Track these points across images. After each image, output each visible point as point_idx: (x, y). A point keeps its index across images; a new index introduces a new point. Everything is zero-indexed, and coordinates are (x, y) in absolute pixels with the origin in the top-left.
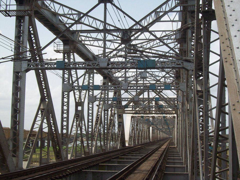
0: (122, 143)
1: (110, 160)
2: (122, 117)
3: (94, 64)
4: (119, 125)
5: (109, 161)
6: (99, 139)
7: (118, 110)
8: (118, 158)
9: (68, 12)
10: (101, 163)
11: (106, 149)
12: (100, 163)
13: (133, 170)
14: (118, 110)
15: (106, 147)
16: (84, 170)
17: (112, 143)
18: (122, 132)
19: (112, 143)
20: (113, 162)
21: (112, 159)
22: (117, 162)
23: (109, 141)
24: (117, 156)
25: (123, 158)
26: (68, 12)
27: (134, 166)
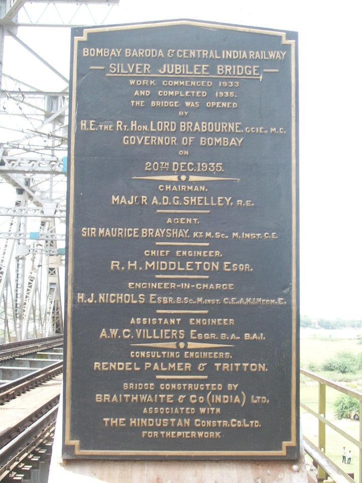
0: (55, 325)
1: (14, 358)
2: (56, 272)
3: (53, 163)
4: (51, 289)
5: (11, 361)
6: (32, 316)
7: (48, 259)
8: (34, 355)
9: (64, 78)
10: (40, 351)
11: (19, 337)
12: (17, 357)
13: (43, 379)
14: (48, 259)
15: (18, 334)
16: (18, 359)
17: (31, 325)
18: (56, 302)
19: (31, 325)
20: (20, 363)
21: (19, 357)
22: (28, 362)
23: (25, 322)
24: (33, 351)
25: (46, 356)
26: (64, 78)
27: (49, 372)
